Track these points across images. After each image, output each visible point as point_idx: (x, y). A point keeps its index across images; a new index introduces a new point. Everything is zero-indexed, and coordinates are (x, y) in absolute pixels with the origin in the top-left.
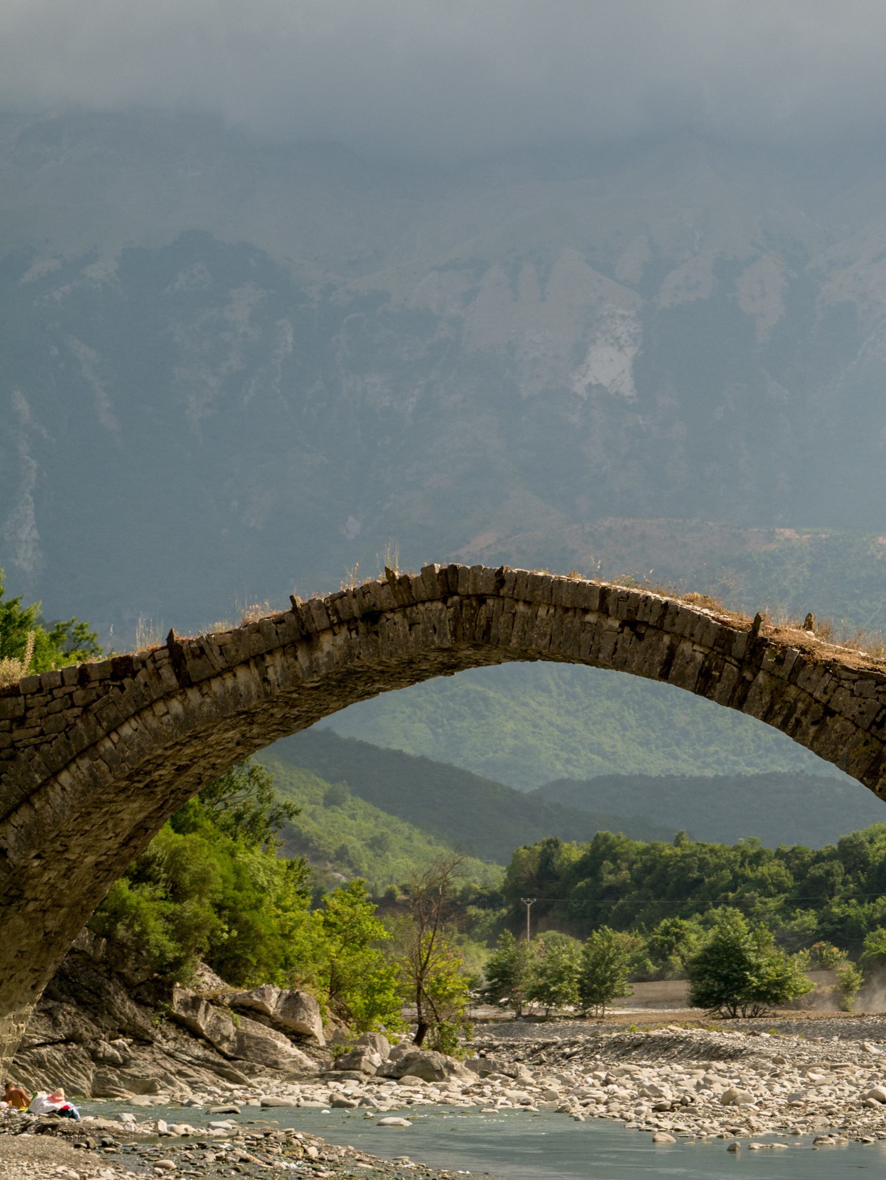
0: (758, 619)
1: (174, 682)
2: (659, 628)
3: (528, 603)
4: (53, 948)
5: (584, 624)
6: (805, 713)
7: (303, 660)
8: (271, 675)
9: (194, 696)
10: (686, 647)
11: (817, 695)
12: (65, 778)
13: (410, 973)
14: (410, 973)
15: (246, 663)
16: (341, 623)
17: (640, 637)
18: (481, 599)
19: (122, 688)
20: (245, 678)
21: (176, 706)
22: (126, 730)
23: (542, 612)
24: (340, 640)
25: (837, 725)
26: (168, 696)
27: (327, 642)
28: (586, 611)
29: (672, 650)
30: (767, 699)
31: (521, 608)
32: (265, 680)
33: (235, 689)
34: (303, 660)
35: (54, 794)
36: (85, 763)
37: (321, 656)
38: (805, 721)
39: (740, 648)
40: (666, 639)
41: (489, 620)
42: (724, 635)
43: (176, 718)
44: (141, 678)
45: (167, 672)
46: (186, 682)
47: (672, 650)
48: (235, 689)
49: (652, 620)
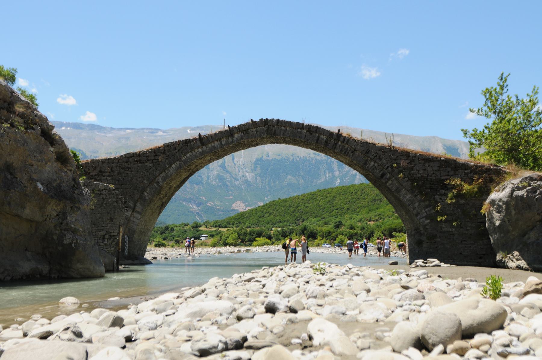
0: (339, 130)
1: (200, 144)
2: (316, 132)
3: (284, 127)
4: (103, 170)
5: (298, 131)
6: (350, 151)
7: (230, 139)
8: (223, 143)
9: (204, 148)
10: (322, 136)
11: (353, 147)
12: (173, 166)
13: (231, 190)
14: (231, 190)
15: (217, 140)
16: (240, 131)
17: (311, 134)
18: (274, 126)
19: (187, 146)
20: (216, 143)
21: (200, 150)
22: (188, 155)
23: (288, 129)
24: (239, 135)
25: (357, 153)
26: (198, 148)
27: (236, 136)
28: (298, 128)
29: (319, 137)
30: (341, 147)
31: (283, 128)
32: (221, 144)
33: (214, 146)
34: (230, 139)
35: (171, 170)
36: (178, 162)
37: (235, 139)
38: (350, 152)
39: (335, 137)
40: (317, 135)
41: (275, 131)
42: (331, 134)
43: (200, 153)
44: (192, 143)
45: (198, 142)
46: (203, 144)
47: (319, 137)
48: (214, 146)
49: (314, 130)
